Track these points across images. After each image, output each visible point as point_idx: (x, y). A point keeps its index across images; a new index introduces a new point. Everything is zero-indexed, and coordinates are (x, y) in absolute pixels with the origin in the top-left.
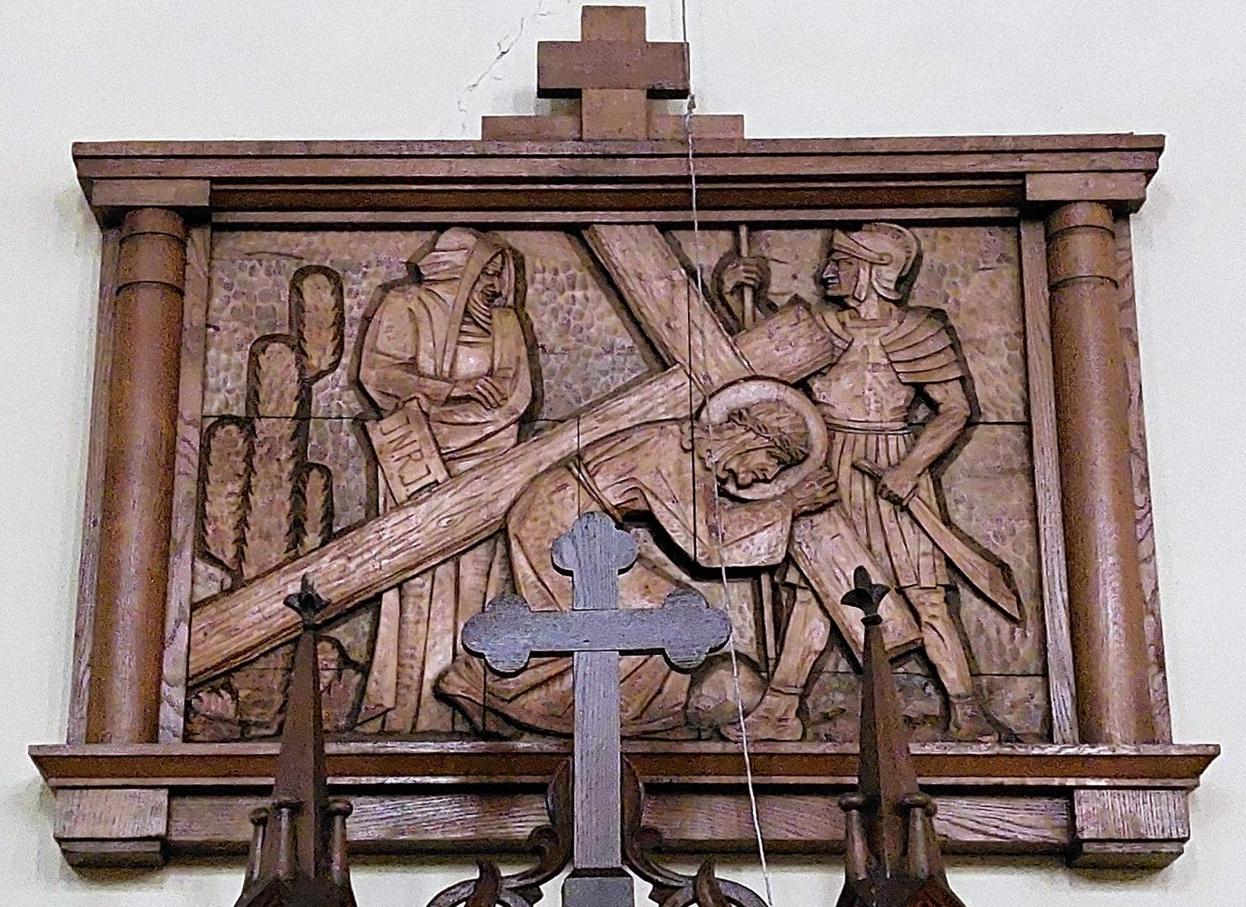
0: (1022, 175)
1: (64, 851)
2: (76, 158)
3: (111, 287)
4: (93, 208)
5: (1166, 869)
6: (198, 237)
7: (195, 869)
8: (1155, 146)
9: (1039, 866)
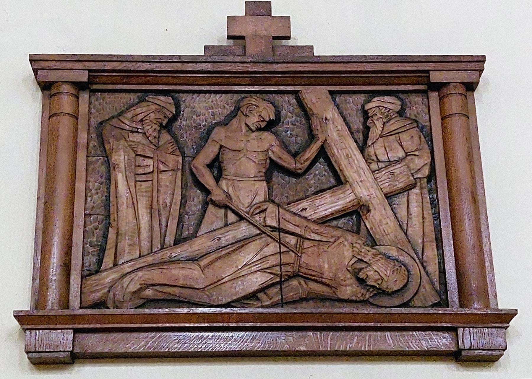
0: (428, 72)
1: (29, 358)
2: (31, 61)
3: (47, 115)
4: (39, 83)
5: (496, 362)
6: (85, 96)
7: (165, 364)
8: (482, 60)
9: (445, 361)
